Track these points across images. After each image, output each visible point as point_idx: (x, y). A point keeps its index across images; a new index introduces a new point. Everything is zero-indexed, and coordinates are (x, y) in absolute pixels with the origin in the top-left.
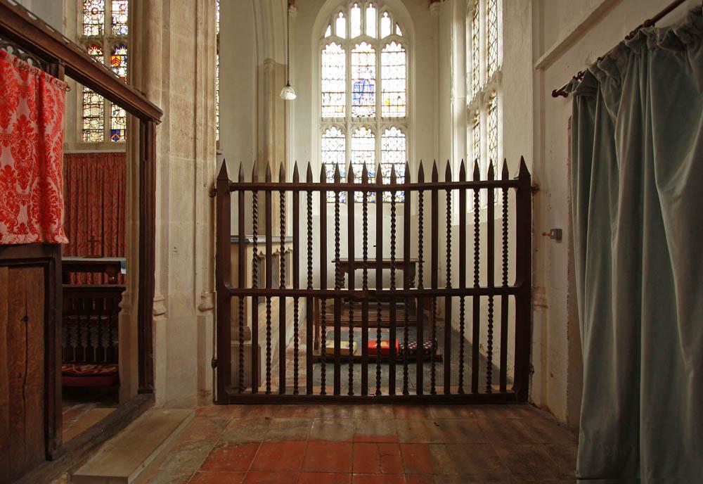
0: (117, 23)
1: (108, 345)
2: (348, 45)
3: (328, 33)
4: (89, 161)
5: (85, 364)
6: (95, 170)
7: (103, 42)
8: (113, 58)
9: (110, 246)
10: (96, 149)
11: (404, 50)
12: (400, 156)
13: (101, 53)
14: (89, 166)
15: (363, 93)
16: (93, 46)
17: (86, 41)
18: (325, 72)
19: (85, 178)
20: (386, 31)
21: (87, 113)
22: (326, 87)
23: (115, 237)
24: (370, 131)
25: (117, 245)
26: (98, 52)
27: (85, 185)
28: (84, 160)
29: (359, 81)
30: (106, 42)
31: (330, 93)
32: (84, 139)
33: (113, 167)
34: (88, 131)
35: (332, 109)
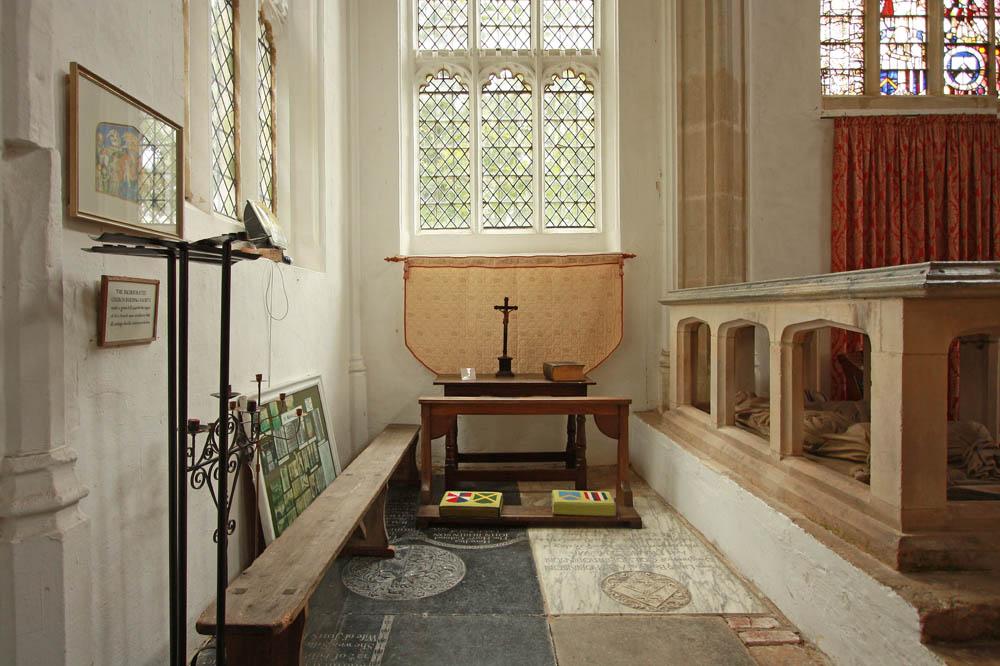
33: (945, 145)
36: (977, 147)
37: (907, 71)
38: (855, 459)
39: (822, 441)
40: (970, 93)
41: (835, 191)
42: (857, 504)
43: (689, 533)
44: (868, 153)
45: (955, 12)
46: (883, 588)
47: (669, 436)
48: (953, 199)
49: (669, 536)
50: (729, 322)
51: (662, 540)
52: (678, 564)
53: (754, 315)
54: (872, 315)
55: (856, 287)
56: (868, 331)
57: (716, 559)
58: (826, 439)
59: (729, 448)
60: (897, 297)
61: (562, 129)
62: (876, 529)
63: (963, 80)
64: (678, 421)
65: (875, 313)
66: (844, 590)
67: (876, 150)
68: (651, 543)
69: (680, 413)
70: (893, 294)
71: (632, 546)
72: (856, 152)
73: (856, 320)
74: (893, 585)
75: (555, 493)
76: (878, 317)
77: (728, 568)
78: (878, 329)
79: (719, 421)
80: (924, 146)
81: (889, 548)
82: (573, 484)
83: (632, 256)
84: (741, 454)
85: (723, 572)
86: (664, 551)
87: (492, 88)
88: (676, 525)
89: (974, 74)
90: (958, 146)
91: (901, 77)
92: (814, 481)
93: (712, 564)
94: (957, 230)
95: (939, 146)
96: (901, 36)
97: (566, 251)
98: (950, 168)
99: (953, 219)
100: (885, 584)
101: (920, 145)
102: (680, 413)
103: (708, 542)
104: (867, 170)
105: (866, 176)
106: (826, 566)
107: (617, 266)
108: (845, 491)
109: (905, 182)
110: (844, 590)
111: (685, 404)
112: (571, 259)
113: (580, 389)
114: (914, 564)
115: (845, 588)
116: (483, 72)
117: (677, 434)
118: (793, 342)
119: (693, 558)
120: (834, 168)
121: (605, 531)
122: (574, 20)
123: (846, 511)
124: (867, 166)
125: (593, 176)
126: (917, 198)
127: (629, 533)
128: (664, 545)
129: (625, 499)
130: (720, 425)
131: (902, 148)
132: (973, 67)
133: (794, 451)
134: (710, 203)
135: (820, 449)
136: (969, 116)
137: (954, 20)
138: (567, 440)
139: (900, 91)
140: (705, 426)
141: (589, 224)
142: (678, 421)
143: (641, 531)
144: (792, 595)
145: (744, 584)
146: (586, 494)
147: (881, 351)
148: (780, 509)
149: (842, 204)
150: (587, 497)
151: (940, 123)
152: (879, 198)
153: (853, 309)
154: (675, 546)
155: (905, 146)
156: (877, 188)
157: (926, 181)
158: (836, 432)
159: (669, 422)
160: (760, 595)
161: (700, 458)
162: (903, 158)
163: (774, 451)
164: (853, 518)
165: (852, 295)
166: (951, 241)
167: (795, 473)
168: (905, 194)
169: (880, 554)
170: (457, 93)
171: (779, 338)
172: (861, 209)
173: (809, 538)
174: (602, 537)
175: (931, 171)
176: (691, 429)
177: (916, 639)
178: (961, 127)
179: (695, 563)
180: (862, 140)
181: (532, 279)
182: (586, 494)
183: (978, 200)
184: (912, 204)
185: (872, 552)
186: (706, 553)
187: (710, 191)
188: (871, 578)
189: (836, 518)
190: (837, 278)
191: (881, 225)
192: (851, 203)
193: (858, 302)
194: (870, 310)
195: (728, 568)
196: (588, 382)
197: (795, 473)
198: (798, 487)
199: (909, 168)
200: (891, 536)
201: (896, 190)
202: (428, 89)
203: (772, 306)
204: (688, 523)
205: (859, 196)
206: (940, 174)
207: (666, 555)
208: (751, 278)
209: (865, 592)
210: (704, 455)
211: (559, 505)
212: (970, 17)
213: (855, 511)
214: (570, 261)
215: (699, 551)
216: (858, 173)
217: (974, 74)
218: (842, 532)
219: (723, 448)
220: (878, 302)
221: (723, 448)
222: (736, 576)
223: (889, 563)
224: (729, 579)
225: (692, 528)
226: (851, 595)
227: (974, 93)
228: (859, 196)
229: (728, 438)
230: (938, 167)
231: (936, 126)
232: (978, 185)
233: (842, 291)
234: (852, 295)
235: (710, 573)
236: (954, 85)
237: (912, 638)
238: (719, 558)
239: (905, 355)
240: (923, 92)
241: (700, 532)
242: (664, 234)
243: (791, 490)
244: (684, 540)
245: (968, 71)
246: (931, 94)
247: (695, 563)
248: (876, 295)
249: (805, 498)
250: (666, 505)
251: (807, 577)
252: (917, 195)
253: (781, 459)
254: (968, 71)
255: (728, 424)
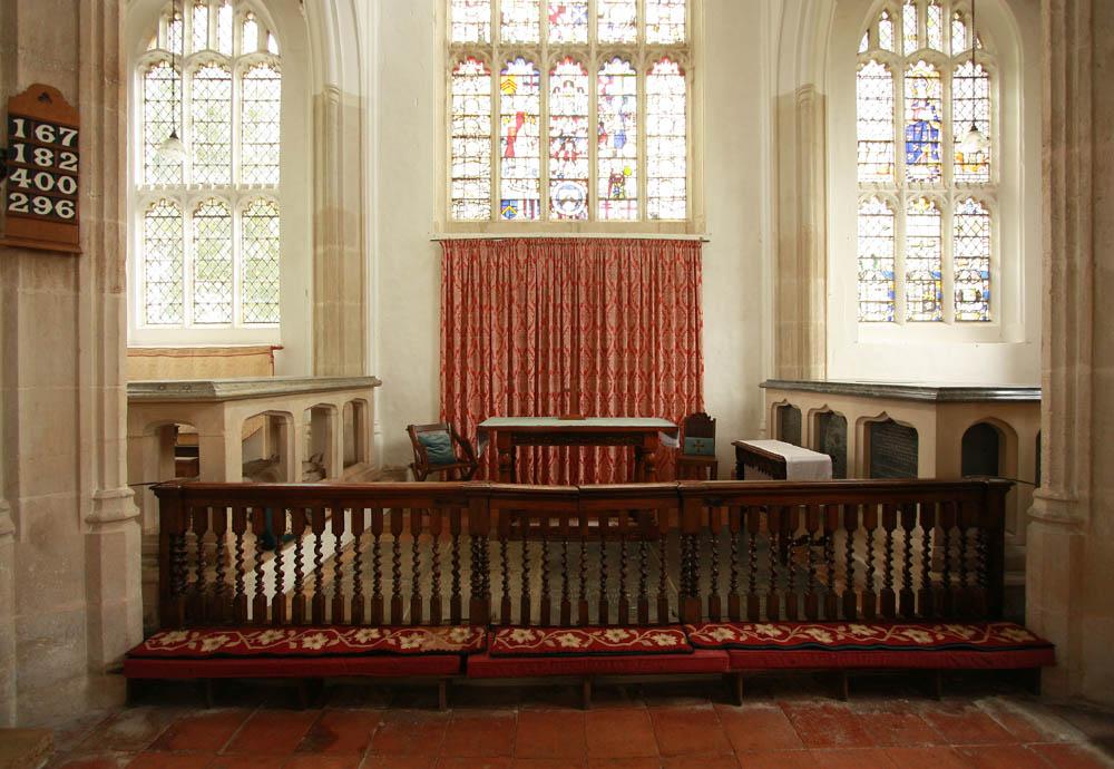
0: (511, 21)
1: (214, 580)
2: (895, 65)
3: (864, 46)
4: (484, 252)
5: (858, 622)
6: (494, 268)
7: (490, 54)
8: (504, 79)
9: (524, 397)
10: (482, 232)
11: (986, 74)
12: (980, 247)
13: (482, 72)
14: (484, 260)
15: (920, 142)
16: (470, 58)
17: (460, 50)
18: (863, 109)
19: (477, 281)
20: (960, 44)
21: (458, 172)
22: (864, 131)
23: (533, 381)
24: (932, 204)
25: (536, 393)
26: (478, 70)
27: (477, 294)
28: (475, 250)
29: (914, 123)
30: (496, 54)
31: (867, 142)
32: (454, 215)
33: (526, 261)
34: (460, 201)
35: (871, 169)
37: (525, 200)
45: (562, 154)
61: (257, 245)
63: (569, 206)
87: (252, 213)
89: (577, 202)
90: (535, 263)
91: (520, 205)
95: (522, 262)
96: (519, 173)
97: (179, 344)
104: (465, 281)
112: (233, 350)
116: (241, 201)
122: (267, 161)
124: (465, 278)
132: (576, 198)
137: (561, 160)
139: (520, 216)
156: (473, 296)
157: (511, 290)
170: (271, 217)
181: (204, 365)
202: (152, 215)
212: (574, 159)
214: (231, 353)
217: (577, 202)
227: (577, 218)
228: (458, 300)
231: (519, 246)
236: (561, 212)
240: (537, 217)
245: (572, 200)
254: (572, 200)
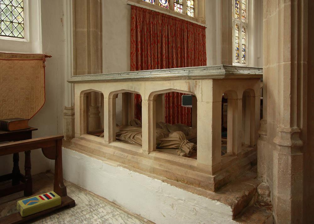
33: (162, 24)
36: (169, 27)
38: (175, 147)
39: (160, 142)
40: (165, 7)
41: (132, 36)
42: (191, 168)
43: (99, 200)
44: (141, 22)
46: (214, 202)
47: (78, 151)
48: (164, 44)
49: (90, 205)
50: (114, 91)
51: (89, 209)
52: (103, 219)
53: (132, 88)
54: (198, 86)
55: (190, 75)
56: (195, 93)
57: (118, 210)
58: (162, 141)
59: (118, 153)
60: (210, 79)
62: (202, 176)
64: (83, 143)
65: (199, 86)
66: (193, 207)
67: (144, 21)
68: (84, 213)
69: (82, 139)
70: (208, 77)
71: (76, 219)
72: (138, 21)
73: (189, 88)
74: (217, 199)
75: (20, 202)
76: (201, 87)
77: (125, 212)
78: (200, 92)
79: (110, 139)
80: (156, 23)
81: (210, 183)
82: (22, 193)
83: (50, 57)
84: (126, 154)
85: (125, 215)
86: (93, 215)
88: (91, 198)
92: (169, 161)
93: (117, 213)
94: (165, 56)
95: (160, 24)
98: (163, 33)
99: (164, 51)
100: (214, 200)
101: (155, 22)
102: (82, 139)
103: (110, 202)
105: (141, 31)
106: (183, 199)
107: (42, 62)
108: (184, 163)
109: (152, 36)
110: (193, 207)
111: (84, 133)
113: (28, 134)
114: (220, 188)
115: (194, 206)
117: (92, 152)
118: (153, 100)
119: (108, 213)
120: (131, 26)
121: (56, 216)
123: (187, 171)
125: (22, 8)
126: (155, 43)
127: (71, 211)
128: (91, 211)
129: (62, 192)
130: (110, 142)
131: (151, 23)
133: (154, 149)
134: (88, 32)
135: (160, 145)
136: (167, 15)
138: (13, 166)
140: (100, 144)
141: (20, 36)
142: (83, 143)
143: (76, 207)
144: (164, 216)
145: (136, 218)
146: (41, 197)
147: (202, 101)
148: (154, 177)
149: (134, 41)
150: (43, 199)
151: (160, 16)
152: (145, 41)
153: (187, 84)
154: (97, 210)
155: (151, 22)
158: (165, 137)
159: (76, 144)
160: (145, 220)
161: (102, 160)
162: (151, 26)
163: (144, 151)
164: (191, 174)
165: (189, 78)
166: (163, 59)
167: (156, 159)
168: (152, 40)
169: (206, 187)
171: (147, 98)
172: (140, 44)
173: (174, 188)
174: (56, 220)
175: (158, 33)
176: (92, 146)
177: (231, 218)
178: (166, 19)
179: (111, 216)
180: (140, 17)
182: (41, 197)
183: (170, 45)
184: (154, 45)
185: (202, 187)
186: (112, 208)
187: (89, 27)
188: (207, 199)
189: (182, 175)
190: (174, 71)
191: (145, 52)
192: (137, 41)
193: (190, 81)
194: (196, 84)
195: (125, 212)
196: (31, 129)
197: (156, 159)
198: (161, 165)
199: (153, 31)
200: (210, 178)
201: (149, 38)
203: (143, 83)
204: (95, 195)
205: (139, 40)
206: (161, 34)
207: (96, 217)
208: (104, 73)
209: (205, 205)
210: (103, 158)
211: (25, 211)
213: (191, 171)
215: (109, 208)
216: (139, 29)
218: (186, 181)
219: (114, 153)
220: (200, 81)
221: (114, 153)
222: (132, 215)
223: (210, 190)
224: (129, 218)
225: (98, 196)
226: (197, 208)
228: (139, 40)
229: (115, 147)
230: (160, 32)
232: (170, 41)
233: (185, 76)
234: (189, 78)
235: (120, 218)
237: (228, 219)
238: (119, 208)
239: (213, 102)
240: (153, 3)
241: (103, 198)
242: (66, 45)
243: (158, 167)
244: (99, 205)
246: (156, 4)
247: (111, 216)
248: (201, 78)
249: (166, 170)
250: (80, 188)
251: (172, 206)
252: (155, 41)
253: (149, 153)
255: (114, 141)
